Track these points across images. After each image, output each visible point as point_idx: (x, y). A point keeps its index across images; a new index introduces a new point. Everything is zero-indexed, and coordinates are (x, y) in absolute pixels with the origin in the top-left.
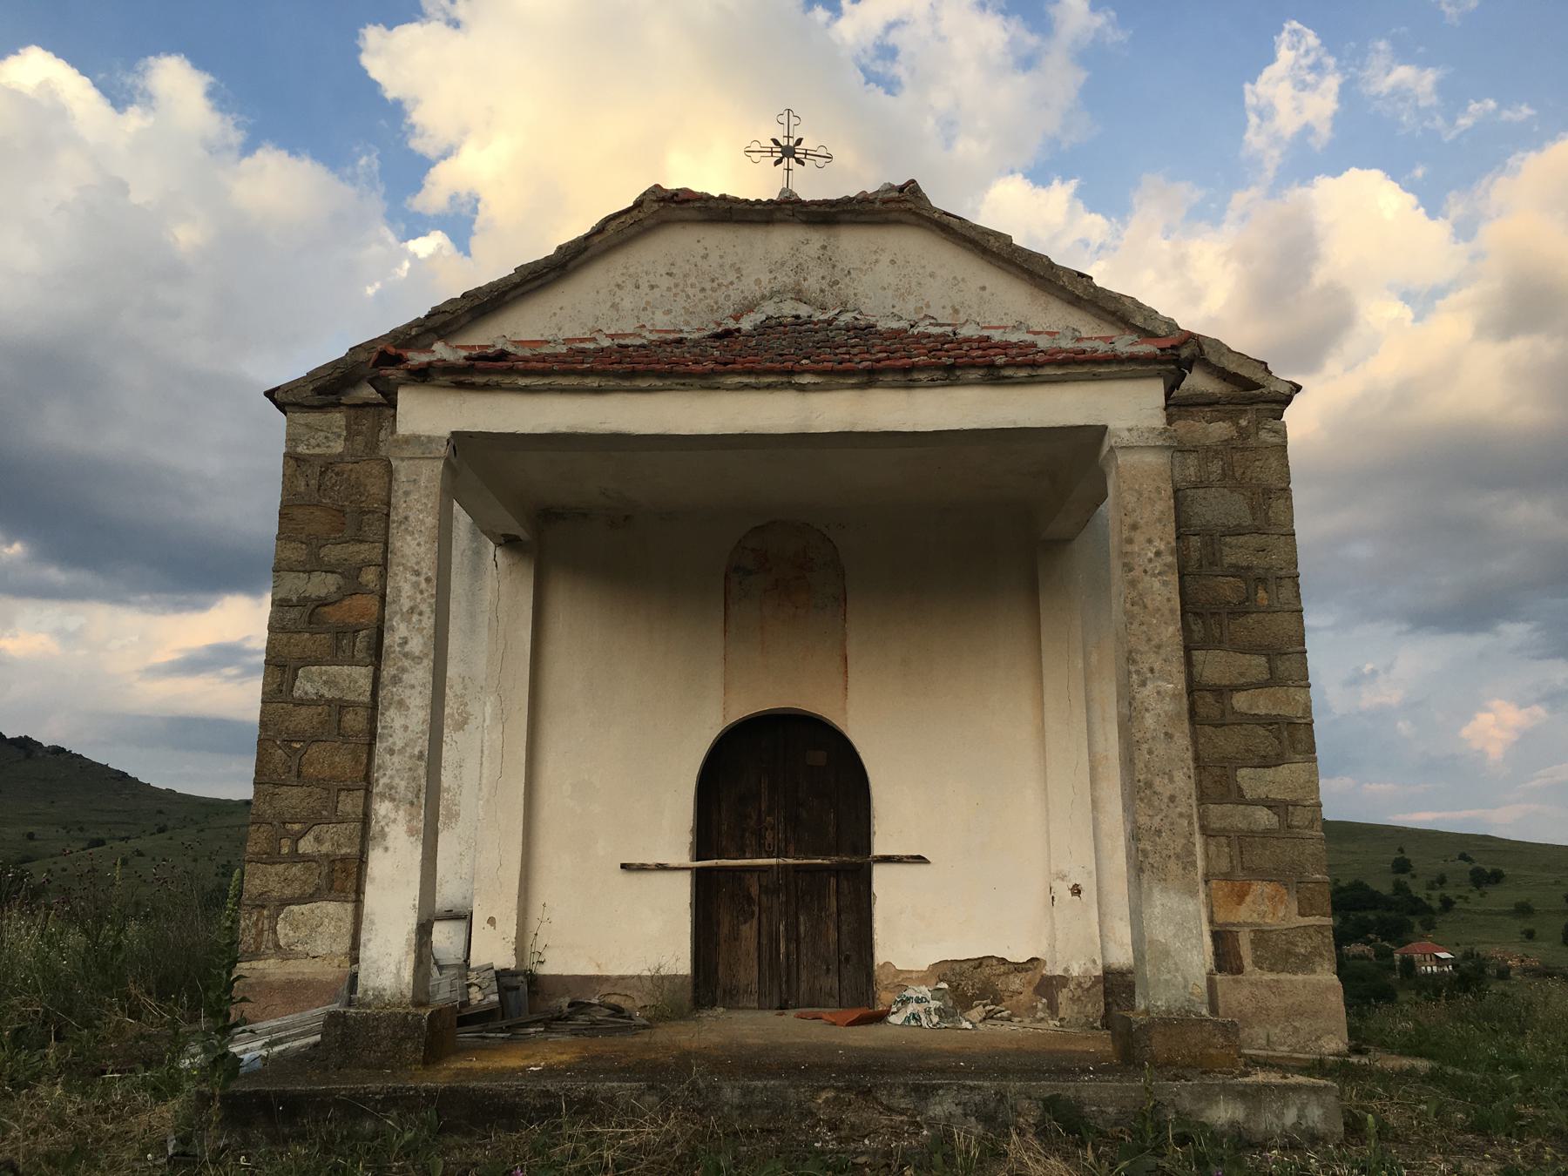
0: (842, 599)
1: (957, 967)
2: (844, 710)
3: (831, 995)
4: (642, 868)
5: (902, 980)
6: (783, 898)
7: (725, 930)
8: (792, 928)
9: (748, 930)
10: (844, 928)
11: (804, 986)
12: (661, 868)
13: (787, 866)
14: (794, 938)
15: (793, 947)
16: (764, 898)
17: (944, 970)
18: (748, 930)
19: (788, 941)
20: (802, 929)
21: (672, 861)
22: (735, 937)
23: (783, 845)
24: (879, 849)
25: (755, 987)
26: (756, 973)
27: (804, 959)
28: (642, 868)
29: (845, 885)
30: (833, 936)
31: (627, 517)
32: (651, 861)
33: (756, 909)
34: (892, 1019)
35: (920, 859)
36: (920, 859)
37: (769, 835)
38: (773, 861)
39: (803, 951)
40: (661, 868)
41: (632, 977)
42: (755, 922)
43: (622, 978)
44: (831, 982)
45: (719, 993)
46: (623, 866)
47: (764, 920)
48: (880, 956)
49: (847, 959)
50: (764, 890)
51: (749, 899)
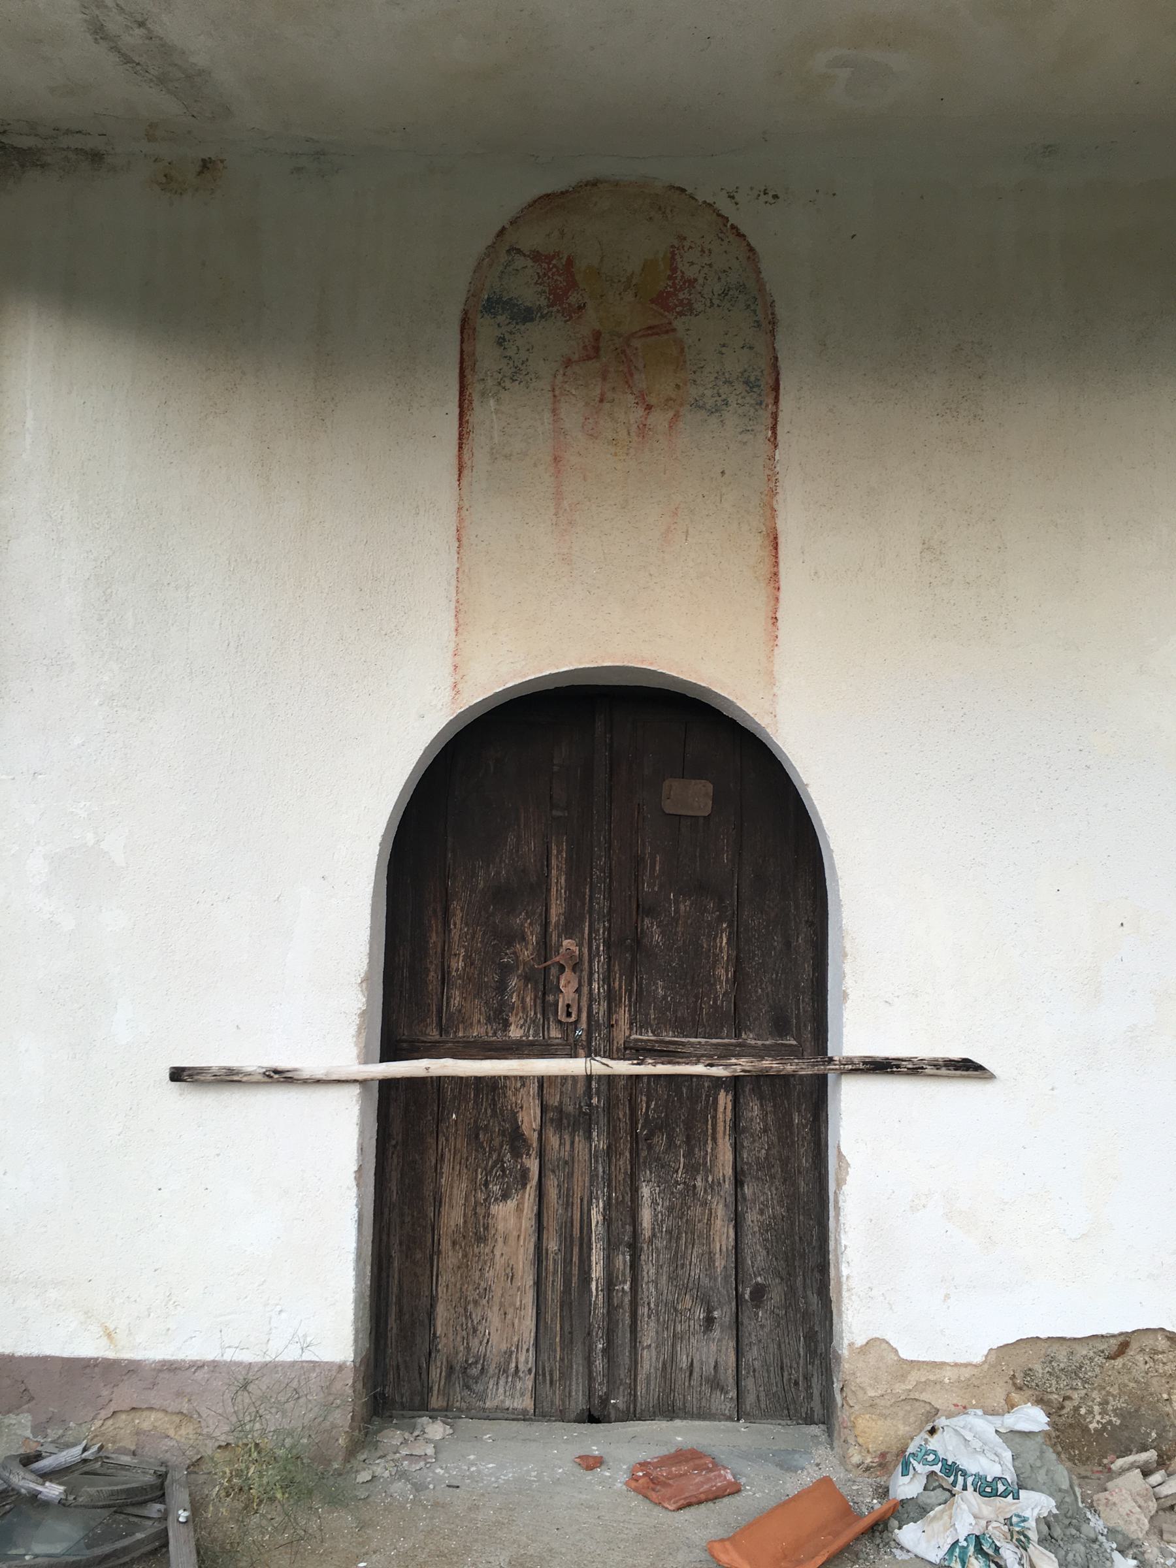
0: (766, 388)
1: (1062, 1354)
2: (771, 679)
3: (716, 1384)
4: (229, 1078)
5: (925, 1396)
6: (600, 1142)
7: (453, 1217)
8: (625, 1211)
9: (512, 1217)
10: (752, 1217)
11: (649, 1361)
12: (279, 1077)
13: (611, 1079)
14: (626, 1237)
15: (622, 1260)
16: (553, 1140)
17: (1037, 1369)
18: (512, 1217)
19: (611, 1248)
20: (646, 1216)
21: (308, 1064)
22: (479, 1232)
23: (601, 1009)
24: (854, 1032)
25: (525, 1359)
26: (529, 1323)
27: (649, 1292)
28: (229, 1078)
29: (754, 1110)
30: (723, 1235)
31: (206, 165)
32: (252, 1061)
33: (533, 1165)
34: (909, 1535)
35: (967, 1067)
36: (967, 1067)
37: (568, 986)
38: (576, 1066)
39: (649, 1270)
40: (279, 1077)
41: (198, 1366)
42: (529, 1195)
43: (170, 1368)
44: (712, 1351)
45: (436, 1374)
46: (177, 1075)
47: (552, 1193)
48: (858, 1320)
49: (759, 1293)
50: (554, 1117)
51: (516, 1139)
